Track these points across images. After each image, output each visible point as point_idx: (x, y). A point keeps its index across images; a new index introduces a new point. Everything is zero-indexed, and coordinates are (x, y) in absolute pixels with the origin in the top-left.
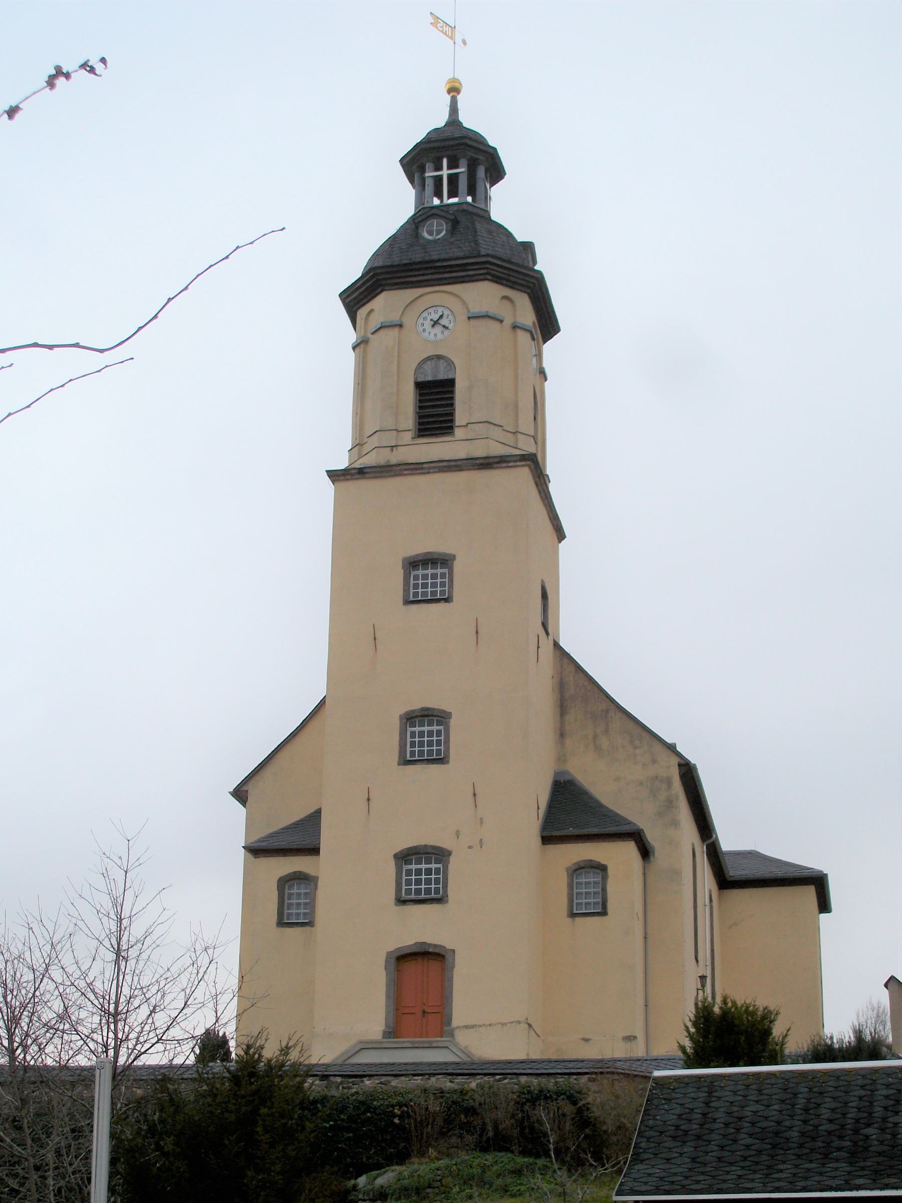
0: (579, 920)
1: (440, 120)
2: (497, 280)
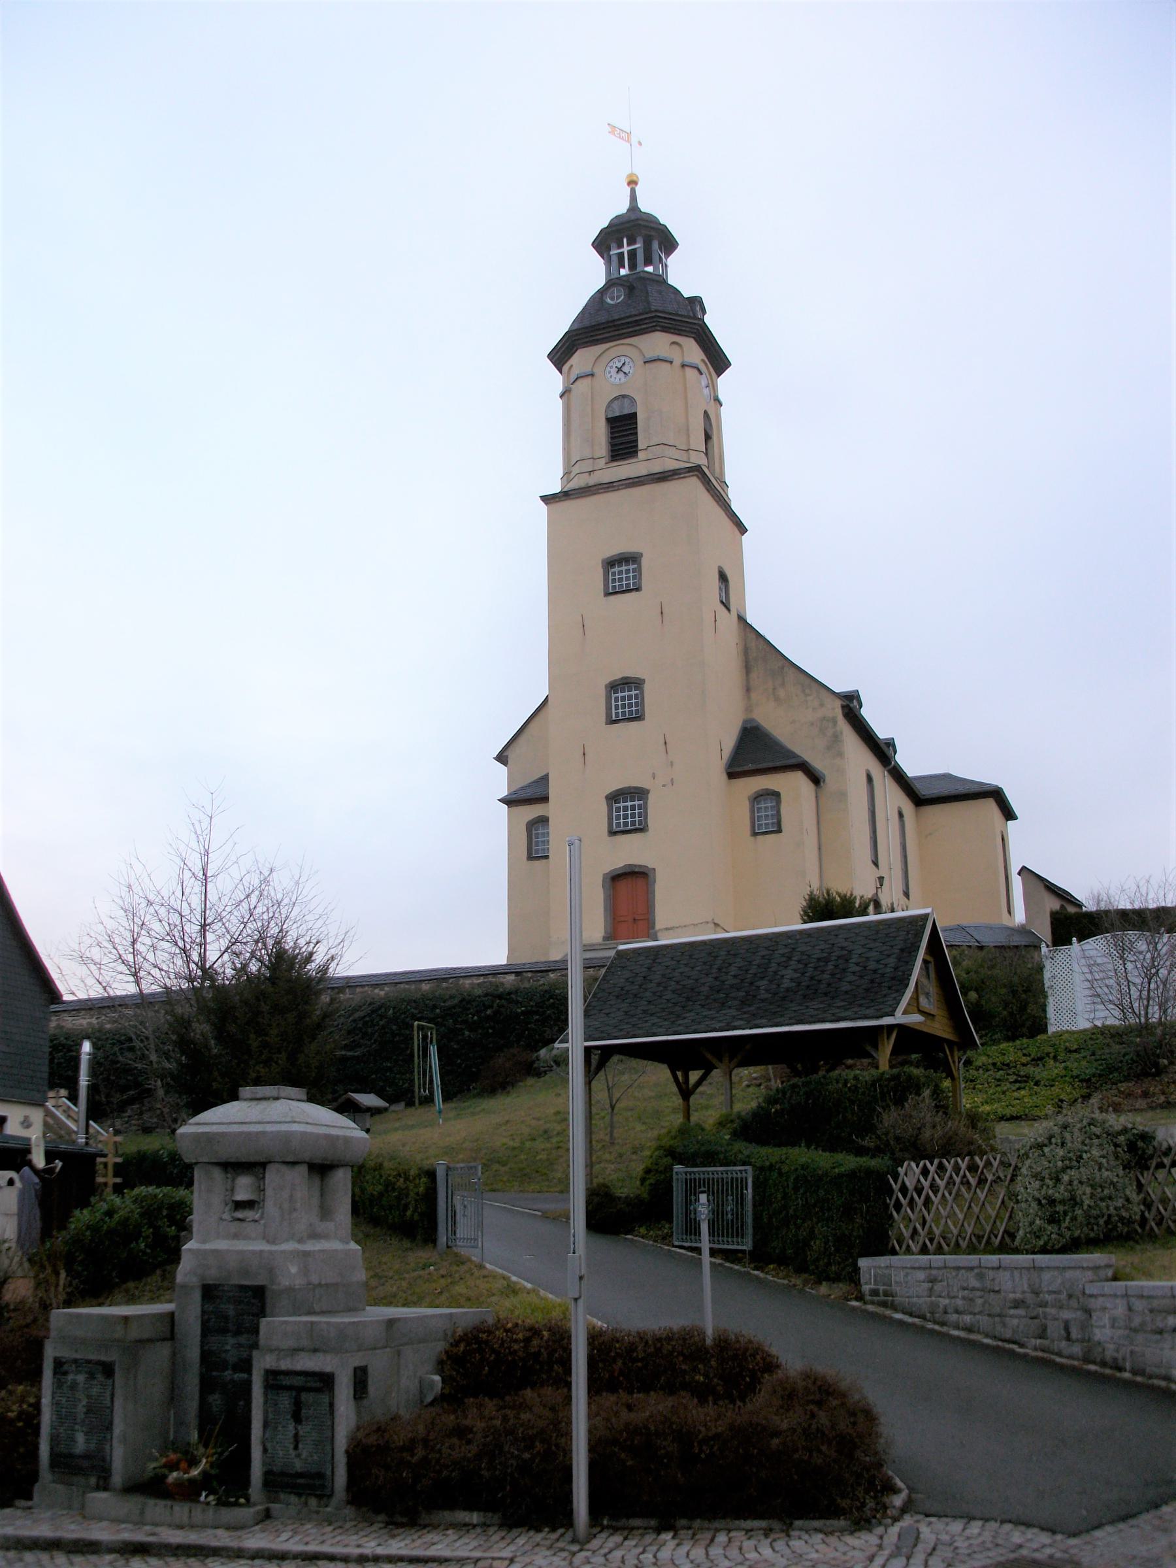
0: (759, 837)
1: (622, 207)
2: (665, 330)
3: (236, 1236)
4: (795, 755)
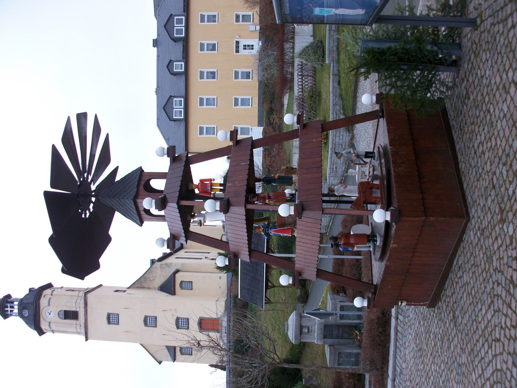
2: (40, 299)
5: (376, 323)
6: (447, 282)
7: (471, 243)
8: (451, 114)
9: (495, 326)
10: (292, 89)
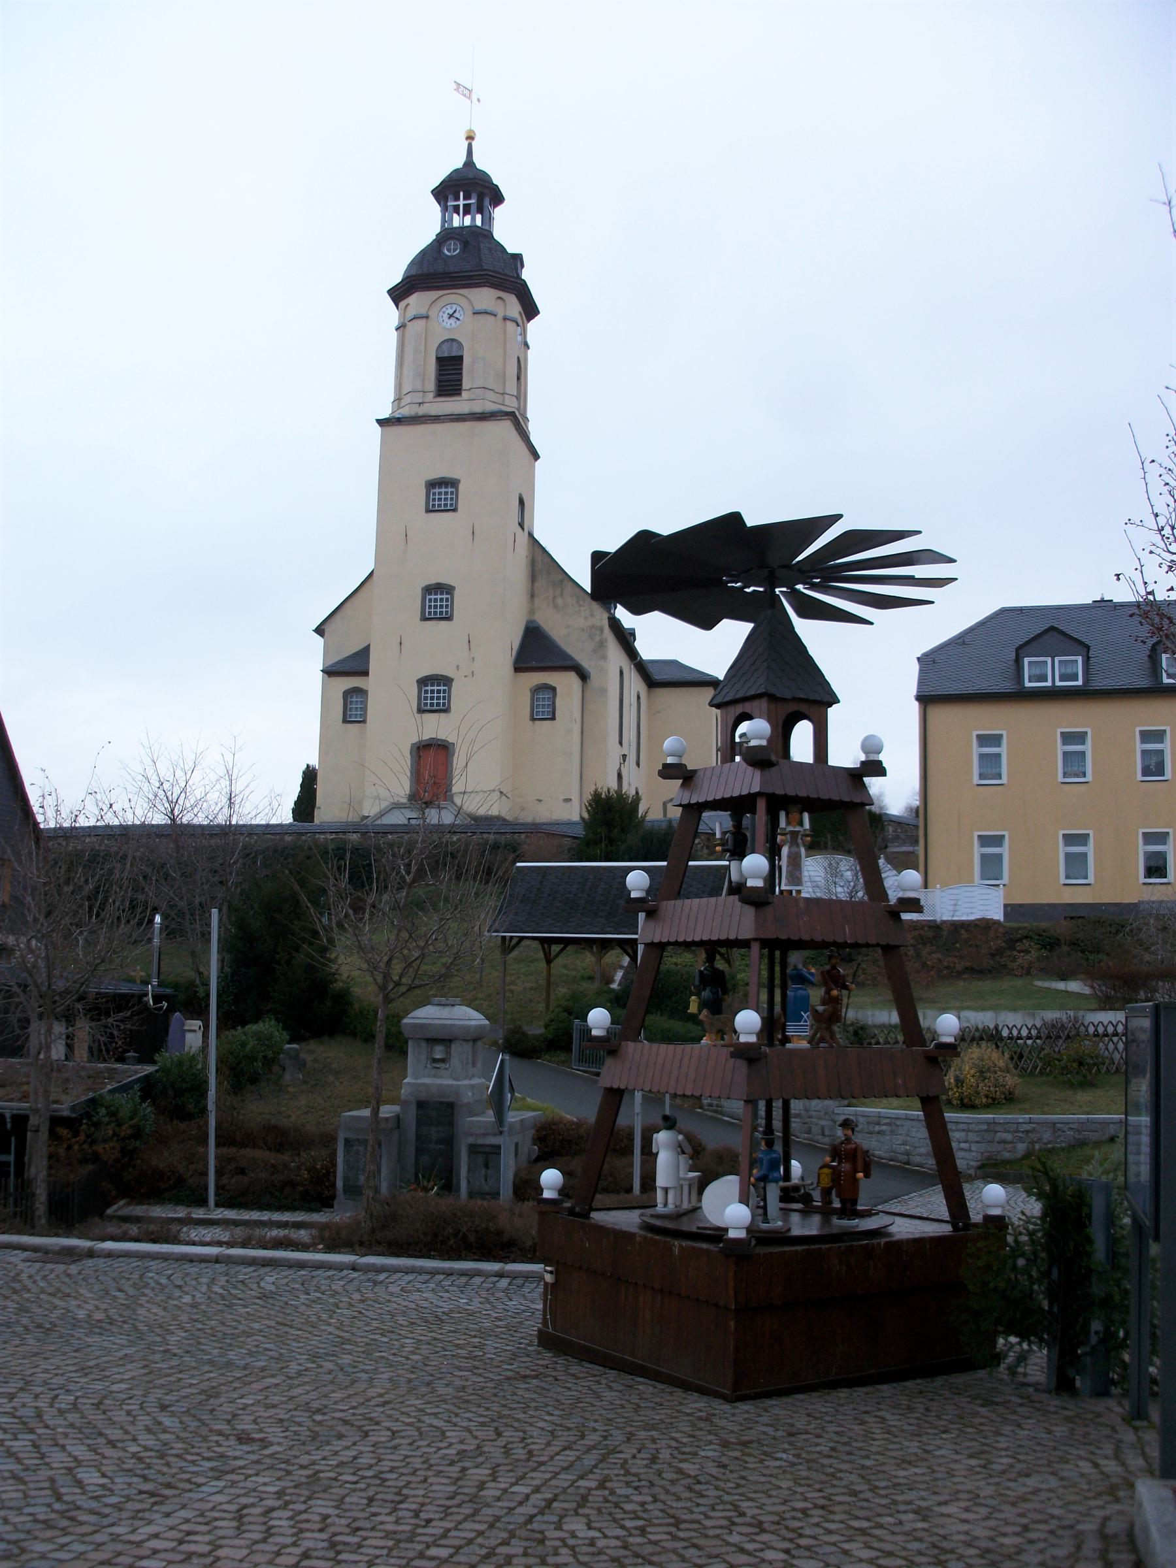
0: (537, 722)
1: (459, 163)
3: (435, 1076)
4: (572, 659)
5: (487, 1228)
6: (597, 1367)
7: (681, 1404)
8: (960, 1379)
9: (524, 1432)
10: (1106, 1003)
